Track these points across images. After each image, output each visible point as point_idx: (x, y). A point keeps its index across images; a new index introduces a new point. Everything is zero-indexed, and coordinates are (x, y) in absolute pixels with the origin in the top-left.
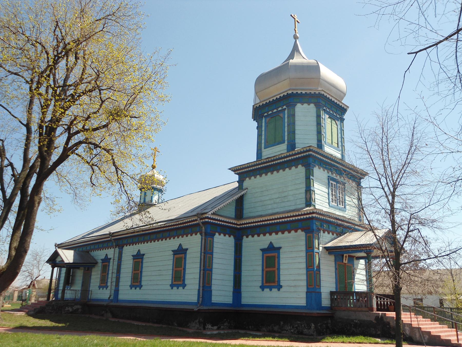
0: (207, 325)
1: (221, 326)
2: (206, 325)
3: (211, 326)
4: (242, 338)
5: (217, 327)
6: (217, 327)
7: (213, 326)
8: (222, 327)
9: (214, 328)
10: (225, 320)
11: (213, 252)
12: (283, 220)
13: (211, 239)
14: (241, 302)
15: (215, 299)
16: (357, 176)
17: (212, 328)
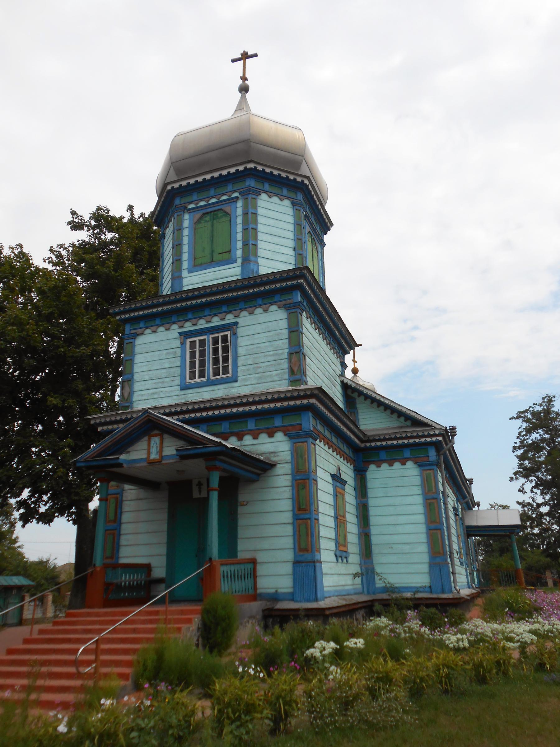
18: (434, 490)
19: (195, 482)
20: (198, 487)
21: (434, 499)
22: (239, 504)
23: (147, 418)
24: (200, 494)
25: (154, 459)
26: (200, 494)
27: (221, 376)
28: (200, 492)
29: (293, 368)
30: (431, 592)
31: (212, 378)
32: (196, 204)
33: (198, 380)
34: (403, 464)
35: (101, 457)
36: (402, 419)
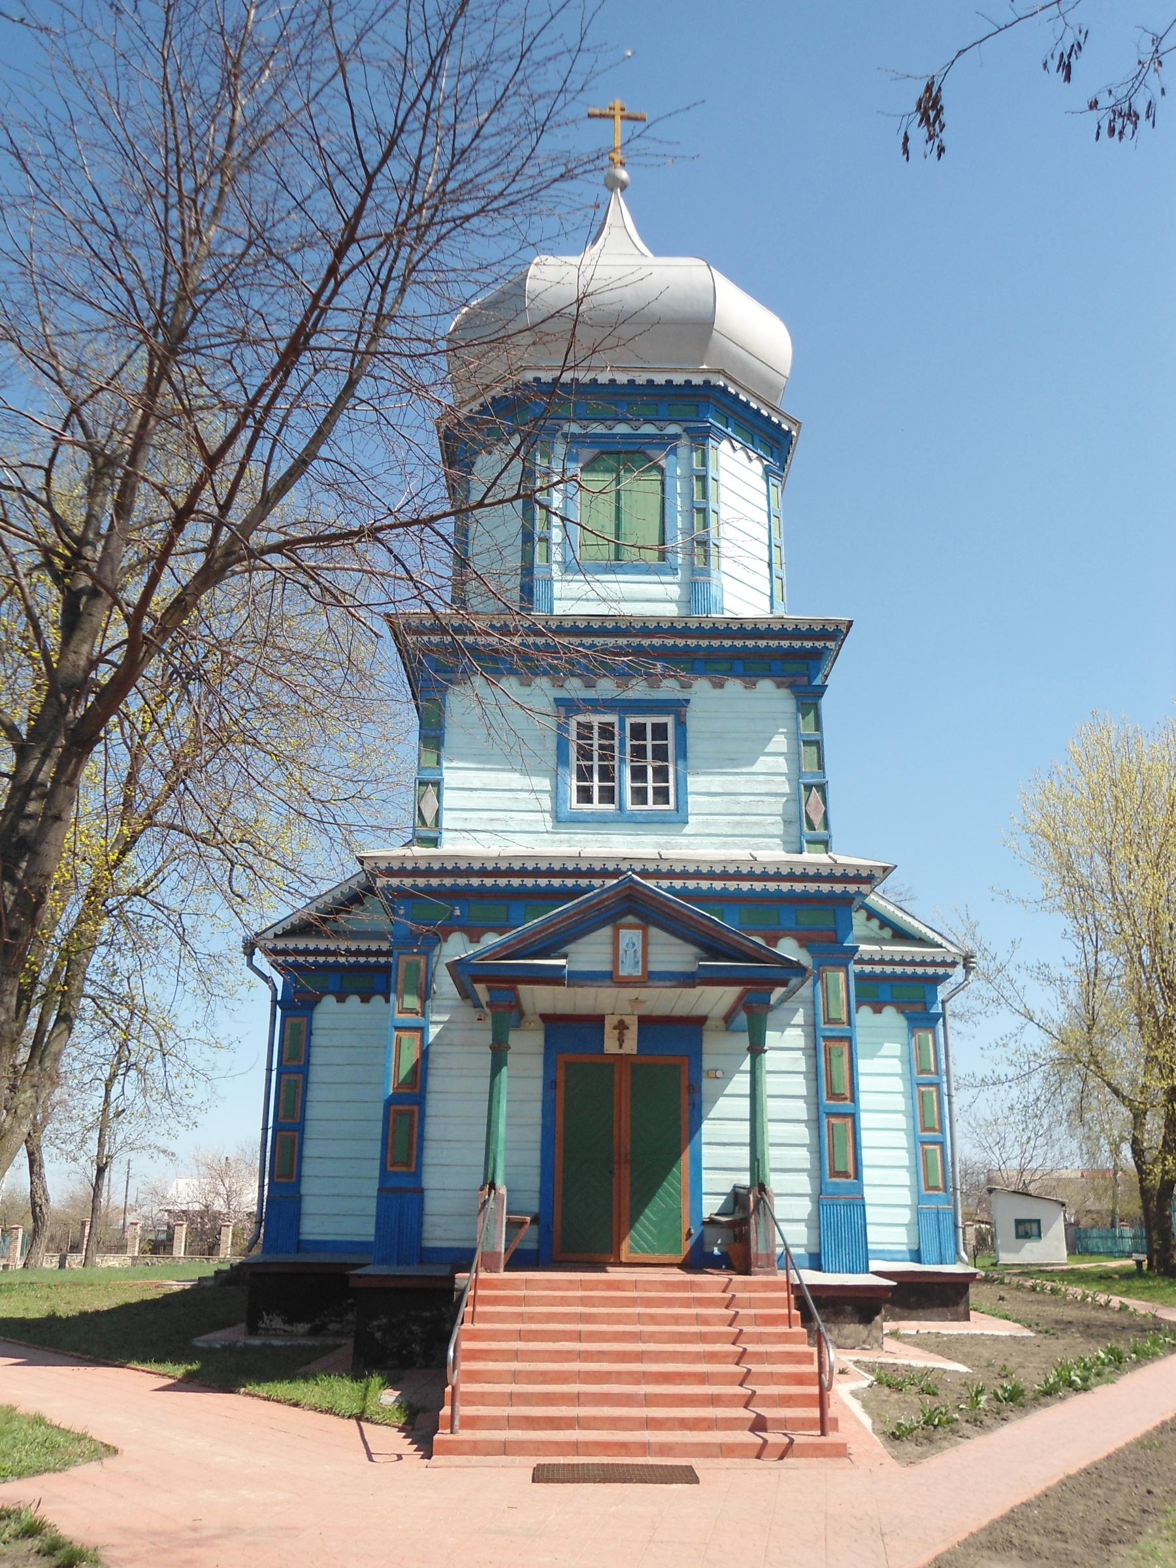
0: (265, 1316)
1: (331, 1321)
2: (262, 1319)
3: (285, 1322)
4: (134, 1364)
5: (307, 1326)
6: (307, 1326)
7: (290, 1322)
8: (331, 1327)
9: (294, 1329)
10: (351, 1301)
11: (308, 1062)
12: (732, 885)
13: (303, 1021)
14: (298, 1233)
15: (312, 1228)
16: (528, 646)
17: (287, 1328)
18: (933, 1069)
19: (610, 1022)
20: (617, 1031)
21: (931, 1084)
22: (704, 1074)
23: (627, 892)
24: (621, 1046)
25: (629, 976)
26: (621, 1046)
27: (650, 805)
28: (621, 1041)
29: (812, 816)
30: (919, 1261)
31: (629, 805)
32: (585, 428)
33: (596, 806)
34: (877, 1010)
35: (548, 957)
36: (875, 923)
